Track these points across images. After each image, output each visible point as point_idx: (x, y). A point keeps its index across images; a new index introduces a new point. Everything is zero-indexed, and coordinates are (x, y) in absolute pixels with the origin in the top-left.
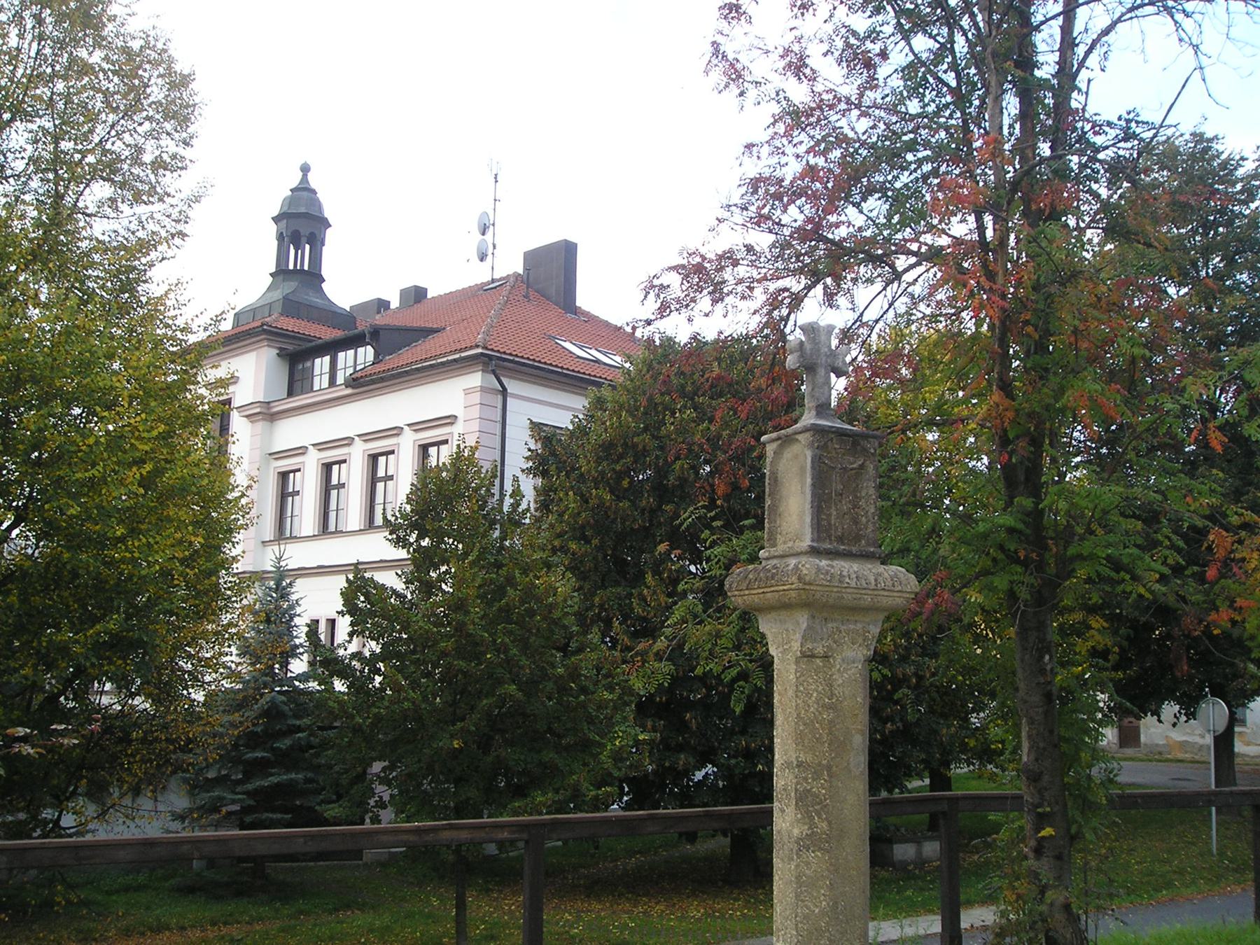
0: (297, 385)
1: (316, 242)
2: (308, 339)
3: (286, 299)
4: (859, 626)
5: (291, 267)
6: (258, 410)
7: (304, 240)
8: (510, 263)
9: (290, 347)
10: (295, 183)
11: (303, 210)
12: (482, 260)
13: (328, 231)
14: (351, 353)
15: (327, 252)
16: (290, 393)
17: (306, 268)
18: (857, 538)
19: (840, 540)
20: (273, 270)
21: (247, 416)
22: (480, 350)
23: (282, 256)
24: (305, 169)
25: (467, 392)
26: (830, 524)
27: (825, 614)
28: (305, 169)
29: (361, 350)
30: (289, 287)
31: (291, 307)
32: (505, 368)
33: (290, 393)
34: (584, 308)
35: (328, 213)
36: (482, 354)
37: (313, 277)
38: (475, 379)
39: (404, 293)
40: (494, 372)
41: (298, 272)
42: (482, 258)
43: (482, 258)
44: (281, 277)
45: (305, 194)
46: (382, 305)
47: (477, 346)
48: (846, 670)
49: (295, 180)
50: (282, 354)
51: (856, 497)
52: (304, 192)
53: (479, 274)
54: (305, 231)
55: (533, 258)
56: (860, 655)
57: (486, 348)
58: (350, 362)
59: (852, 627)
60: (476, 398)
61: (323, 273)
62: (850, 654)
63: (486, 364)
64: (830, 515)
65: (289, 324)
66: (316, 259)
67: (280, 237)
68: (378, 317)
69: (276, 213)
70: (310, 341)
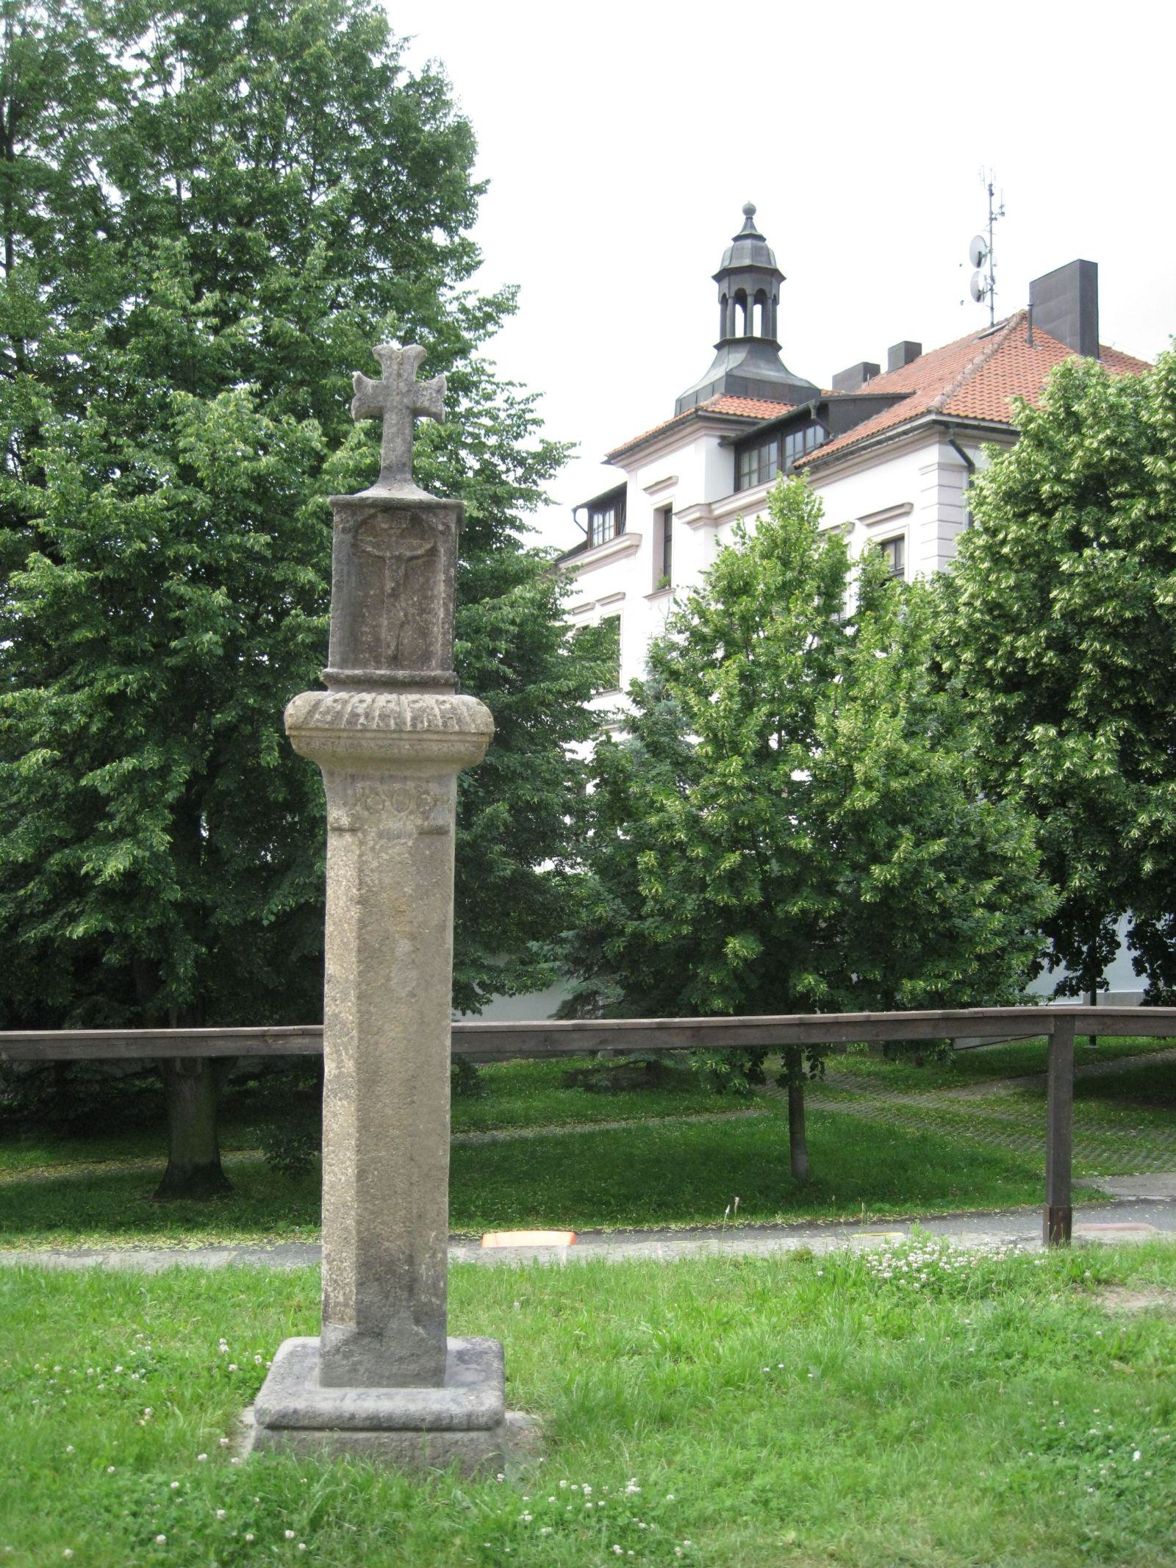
0: (745, 481)
1: (767, 299)
2: (751, 422)
3: (729, 375)
4: (410, 785)
5: (739, 333)
6: (697, 515)
7: (750, 300)
8: (1013, 299)
9: (732, 434)
10: (737, 231)
11: (747, 262)
12: (978, 299)
13: (783, 285)
14: (799, 435)
15: (781, 310)
16: (738, 488)
17: (757, 332)
18: (425, 657)
19: (395, 661)
20: (717, 340)
21: (689, 523)
22: (933, 417)
23: (727, 322)
24: (749, 212)
25: (924, 470)
26: (378, 640)
27: (350, 770)
28: (749, 212)
29: (810, 431)
30: (736, 358)
31: (735, 385)
32: (966, 436)
33: (738, 488)
34: (1117, 348)
35: (781, 267)
36: (935, 422)
37: (767, 346)
38: (932, 454)
39: (893, 352)
40: (953, 443)
41: (748, 340)
42: (979, 296)
43: (979, 296)
44: (725, 350)
45: (748, 243)
46: (870, 370)
47: (929, 412)
48: (383, 849)
49: (737, 226)
50: (724, 442)
51: (426, 597)
52: (750, 236)
53: (977, 319)
54: (750, 290)
55: (1042, 289)
56: (410, 826)
57: (941, 413)
58: (799, 447)
59: (397, 786)
60: (934, 478)
61: (780, 340)
62: (393, 825)
63: (943, 434)
64: (378, 626)
65: (733, 406)
66: (770, 322)
67: (724, 300)
68: (864, 385)
69: (716, 270)
70: (754, 424)
